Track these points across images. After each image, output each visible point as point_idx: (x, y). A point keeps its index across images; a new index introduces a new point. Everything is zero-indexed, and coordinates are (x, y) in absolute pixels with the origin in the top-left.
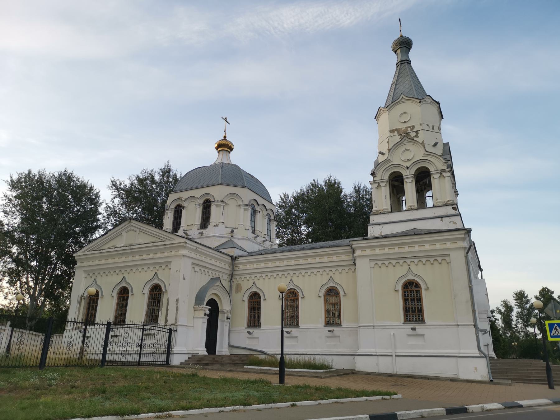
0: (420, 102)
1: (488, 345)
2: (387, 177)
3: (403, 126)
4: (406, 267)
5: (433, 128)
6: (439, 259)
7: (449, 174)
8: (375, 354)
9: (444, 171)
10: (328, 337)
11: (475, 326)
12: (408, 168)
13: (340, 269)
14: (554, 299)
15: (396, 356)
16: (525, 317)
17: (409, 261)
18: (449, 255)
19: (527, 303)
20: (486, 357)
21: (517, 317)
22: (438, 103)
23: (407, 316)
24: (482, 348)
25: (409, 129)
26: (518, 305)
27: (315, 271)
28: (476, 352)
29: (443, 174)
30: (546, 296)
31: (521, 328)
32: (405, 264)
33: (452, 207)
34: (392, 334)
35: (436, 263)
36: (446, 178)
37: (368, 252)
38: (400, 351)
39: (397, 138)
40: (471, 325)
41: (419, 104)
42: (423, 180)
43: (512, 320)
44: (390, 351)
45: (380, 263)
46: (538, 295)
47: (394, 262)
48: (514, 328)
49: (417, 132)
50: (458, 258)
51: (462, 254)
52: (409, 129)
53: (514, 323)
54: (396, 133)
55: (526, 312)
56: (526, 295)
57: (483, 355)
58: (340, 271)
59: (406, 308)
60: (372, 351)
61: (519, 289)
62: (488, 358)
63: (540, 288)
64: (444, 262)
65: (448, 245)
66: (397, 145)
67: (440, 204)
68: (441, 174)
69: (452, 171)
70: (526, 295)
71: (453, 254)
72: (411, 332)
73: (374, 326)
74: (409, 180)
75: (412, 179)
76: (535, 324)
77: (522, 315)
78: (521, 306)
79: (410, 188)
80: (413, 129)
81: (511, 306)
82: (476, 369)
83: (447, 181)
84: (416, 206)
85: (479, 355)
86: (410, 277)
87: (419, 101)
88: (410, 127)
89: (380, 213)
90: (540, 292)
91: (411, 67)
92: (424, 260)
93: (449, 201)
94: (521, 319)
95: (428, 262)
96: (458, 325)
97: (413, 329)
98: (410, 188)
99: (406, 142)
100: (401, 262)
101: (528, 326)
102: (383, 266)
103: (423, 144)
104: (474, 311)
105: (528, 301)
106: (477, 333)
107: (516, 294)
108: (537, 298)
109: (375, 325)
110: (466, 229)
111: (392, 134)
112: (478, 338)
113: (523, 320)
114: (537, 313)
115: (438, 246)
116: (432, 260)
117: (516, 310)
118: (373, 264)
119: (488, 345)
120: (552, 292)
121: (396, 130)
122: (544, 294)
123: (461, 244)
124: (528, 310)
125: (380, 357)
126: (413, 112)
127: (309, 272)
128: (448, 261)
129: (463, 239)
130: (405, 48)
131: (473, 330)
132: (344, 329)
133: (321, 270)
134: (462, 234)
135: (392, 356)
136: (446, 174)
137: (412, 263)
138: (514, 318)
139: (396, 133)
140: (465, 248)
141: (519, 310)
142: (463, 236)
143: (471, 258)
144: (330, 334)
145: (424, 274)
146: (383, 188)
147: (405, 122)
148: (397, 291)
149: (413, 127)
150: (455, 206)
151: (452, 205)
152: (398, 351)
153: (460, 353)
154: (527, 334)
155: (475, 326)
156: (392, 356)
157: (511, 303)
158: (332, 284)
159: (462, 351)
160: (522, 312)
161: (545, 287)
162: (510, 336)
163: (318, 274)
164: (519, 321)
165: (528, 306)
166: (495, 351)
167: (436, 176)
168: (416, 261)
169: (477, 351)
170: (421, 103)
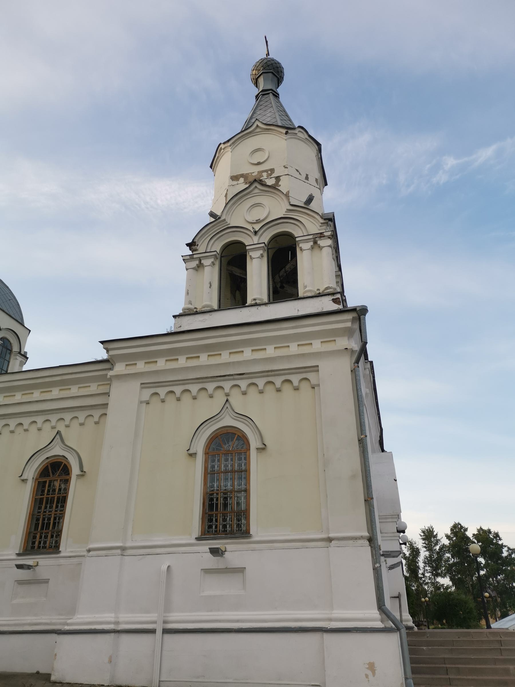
0: (287, 133)
1: (398, 597)
2: (217, 247)
3: (254, 171)
4: (220, 399)
5: (307, 178)
6: (295, 379)
7: (329, 242)
8: (111, 627)
9: (321, 235)
10: (21, 582)
11: (371, 540)
12: (256, 233)
13: (82, 416)
14: (468, 538)
15: (166, 631)
16: (435, 563)
17: (227, 385)
18: (315, 369)
19: (436, 544)
20: (398, 629)
21: (425, 563)
22: (319, 145)
23: (211, 520)
24: (388, 604)
25: (265, 174)
26: (425, 547)
27: (26, 421)
28: (371, 616)
29: (319, 242)
30: (459, 535)
31: (430, 579)
32: (219, 392)
33: (331, 298)
34: (164, 567)
35: (287, 388)
36: (324, 249)
37: (141, 366)
38: (179, 618)
39: (241, 185)
40: (362, 538)
41: (285, 137)
42: (283, 257)
43: (418, 567)
44: (153, 616)
45: (162, 391)
46: (449, 532)
47: (194, 388)
48: (421, 578)
49: (278, 178)
50: (335, 373)
51: (345, 364)
52: (265, 174)
53: (421, 572)
54: (242, 180)
55: (436, 556)
56: (435, 534)
57: (391, 624)
58: (81, 420)
59: (211, 500)
60: (105, 618)
61: (426, 525)
62: (404, 631)
63: (452, 524)
64: (305, 385)
65: (317, 346)
66: (240, 196)
67: (309, 294)
68: (315, 242)
69: (334, 236)
70: (435, 534)
71: (326, 367)
72: (211, 561)
73: (123, 549)
74: (255, 254)
75: (261, 252)
76: (479, 554)
77: (431, 560)
78: (429, 548)
79: (257, 275)
80: (271, 174)
81: (417, 548)
82: (371, 667)
83: (327, 253)
84: (266, 300)
85: (379, 625)
86: (228, 421)
87: (284, 131)
88: (266, 171)
89: (196, 313)
90: (452, 530)
91: (279, 102)
92: (261, 382)
93: (327, 288)
94: (429, 566)
95: (270, 387)
96: (330, 540)
97: (215, 552)
98: (257, 275)
99: (256, 191)
100: (211, 387)
101: (437, 575)
102: (171, 399)
103: (287, 195)
104: (368, 500)
105: (438, 541)
106: (375, 559)
107: (423, 532)
108: (448, 537)
109: (129, 544)
110: (354, 310)
111: (235, 183)
112: (377, 572)
113: (432, 567)
114: (449, 558)
115: (294, 349)
116: (278, 381)
117: (424, 554)
118: (147, 394)
119: (398, 597)
120: (466, 530)
121: (242, 176)
122: (457, 532)
123: (343, 343)
124: (438, 553)
125: (125, 638)
126: (275, 149)
127: (13, 423)
128: (314, 381)
129: (348, 333)
130: (270, 74)
131: (366, 551)
132: (62, 561)
133: (40, 420)
134: (345, 321)
135: (153, 631)
136: (322, 242)
137: (235, 391)
138: (421, 565)
139: (242, 180)
140: (352, 351)
141: (427, 554)
142: (349, 324)
143: (366, 394)
144: (23, 574)
145: (262, 413)
146: (206, 269)
147: (259, 164)
148: (192, 455)
149: (272, 170)
150: (339, 296)
151: (333, 294)
152: (174, 616)
153: (330, 620)
154: (437, 587)
155: (371, 540)
156: (153, 631)
157: (417, 543)
158: (57, 451)
159: (337, 613)
160: (430, 556)
161: (457, 522)
162: (416, 590)
163: (33, 429)
164: (428, 568)
165: (437, 548)
166: (412, 614)
167: (306, 246)
168: (243, 384)
169: (375, 613)
170: (288, 136)
